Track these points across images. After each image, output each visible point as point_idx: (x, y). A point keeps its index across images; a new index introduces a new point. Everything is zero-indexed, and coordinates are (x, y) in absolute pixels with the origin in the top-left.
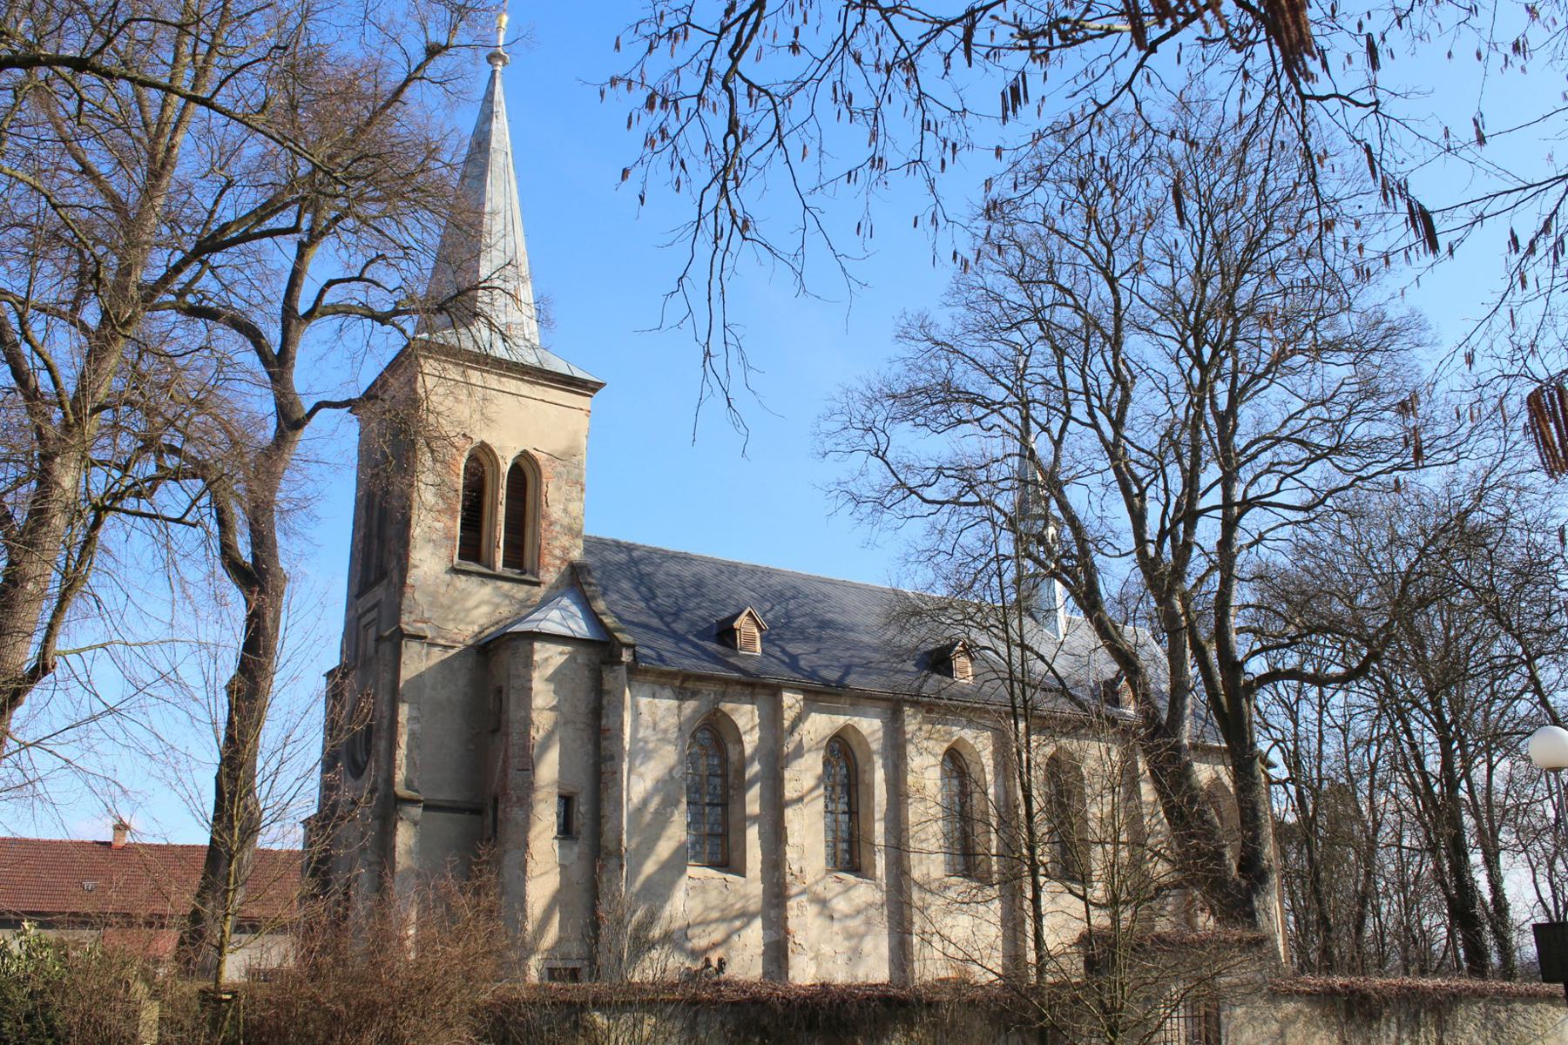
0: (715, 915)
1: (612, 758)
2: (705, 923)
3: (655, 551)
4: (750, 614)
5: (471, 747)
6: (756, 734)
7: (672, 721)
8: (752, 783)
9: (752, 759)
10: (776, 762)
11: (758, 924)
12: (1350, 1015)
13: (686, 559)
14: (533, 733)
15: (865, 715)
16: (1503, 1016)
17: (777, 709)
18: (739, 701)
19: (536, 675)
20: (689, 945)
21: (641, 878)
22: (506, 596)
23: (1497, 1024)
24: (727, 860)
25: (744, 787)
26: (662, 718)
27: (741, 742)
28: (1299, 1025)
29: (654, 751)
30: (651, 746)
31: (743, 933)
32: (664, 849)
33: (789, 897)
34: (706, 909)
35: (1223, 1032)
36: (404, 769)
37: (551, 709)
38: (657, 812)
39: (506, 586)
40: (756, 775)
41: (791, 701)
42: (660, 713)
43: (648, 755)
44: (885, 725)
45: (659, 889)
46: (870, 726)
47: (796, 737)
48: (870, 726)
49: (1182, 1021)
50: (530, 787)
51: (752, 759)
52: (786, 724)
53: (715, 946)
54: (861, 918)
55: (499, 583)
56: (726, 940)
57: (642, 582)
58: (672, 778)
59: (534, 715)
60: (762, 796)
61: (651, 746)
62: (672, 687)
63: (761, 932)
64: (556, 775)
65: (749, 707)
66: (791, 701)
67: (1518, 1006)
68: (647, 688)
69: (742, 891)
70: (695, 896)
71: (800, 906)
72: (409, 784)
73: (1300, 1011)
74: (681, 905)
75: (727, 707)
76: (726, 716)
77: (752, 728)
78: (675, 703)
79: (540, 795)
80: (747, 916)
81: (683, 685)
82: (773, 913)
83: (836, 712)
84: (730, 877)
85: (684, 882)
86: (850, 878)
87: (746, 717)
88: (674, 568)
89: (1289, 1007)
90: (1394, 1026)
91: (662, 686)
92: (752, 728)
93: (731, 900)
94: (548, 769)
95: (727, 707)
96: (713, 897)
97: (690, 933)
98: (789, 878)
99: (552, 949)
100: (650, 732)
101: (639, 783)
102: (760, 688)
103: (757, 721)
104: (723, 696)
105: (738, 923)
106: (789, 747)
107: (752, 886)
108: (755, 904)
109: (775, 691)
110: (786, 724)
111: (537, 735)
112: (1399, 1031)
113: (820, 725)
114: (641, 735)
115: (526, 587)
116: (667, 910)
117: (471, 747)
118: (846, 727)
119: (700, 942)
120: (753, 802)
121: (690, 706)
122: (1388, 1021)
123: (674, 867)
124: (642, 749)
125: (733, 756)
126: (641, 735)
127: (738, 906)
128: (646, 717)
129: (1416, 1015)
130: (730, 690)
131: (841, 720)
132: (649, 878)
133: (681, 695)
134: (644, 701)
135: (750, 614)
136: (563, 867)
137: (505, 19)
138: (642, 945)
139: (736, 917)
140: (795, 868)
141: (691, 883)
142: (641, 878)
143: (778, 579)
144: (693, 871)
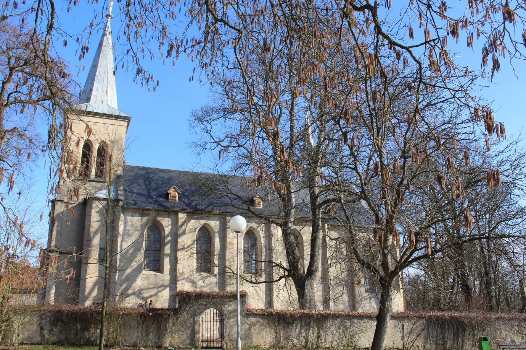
0: (152, 286)
1: (115, 236)
2: (149, 289)
3: (157, 169)
4: (174, 188)
5: (79, 234)
6: (170, 227)
7: (139, 224)
8: (167, 243)
9: (168, 236)
10: (175, 236)
11: (168, 289)
12: (279, 323)
13: (168, 171)
14: (91, 229)
15: (212, 220)
16: (348, 324)
17: (177, 219)
18: (164, 217)
19: (93, 211)
20: (142, 296)
21: (125, 275)
22: (93, 187)
23: (345, 327)
24: (159, 269)
25: (165, 245)
26: (135, 223)
27: (164, 230)
28: (258, 326)
29: (132, 233)
30: (131, 232)
31: (162, 292)
32: (134, 265)
33: (178, 281)
34: (149, 284)
35: (225, 327)
36: (54, 241)
37: (98, 221)
38: (132, 253)
39: (94, 183)
40: (169, 241)
41: (182, 216)
42: (134, 221)
43: (129, 235)
44: (220, 222)
45: (131, 278)
46: (214, 224)
47: (183, 228)
48: (214, 224)
49: (218, 323)
50: (90, 246)
51: (168, 236)
52: (180, 224)
53: (151, 296)
54: (209, 287)
55: (91, 183)
56: (156, 294)
57: (147, 179)
58: (138, 242)
59: (92, 224)
60: (171, 247)
61: (131, 232)
62: (139, 213)
63: (169, 292)
64: (99, 242)
65: (167, 218)
66: (182, 216)
67: (356, 321)
68: (130, 213)
69: (162, 279)
70: (145, 279)
71: (182, 284)
72: (56, 247)
73: (258, 321)
74: (139, 283)
75: (159, 219)
76: (159, 222)
77: (168, 226)
78: (140, 218)
79: (94, 248)
80: (164, 287)
81: (143, 212)
82: (173, 286)
83: (202, 219)
84: (158, 274)
85: (141, 276)
86: (205, 274)
87: (166, 222)
88: (162, 174)
89: (253, 320)
90: (299, 327)
91: (135, 213)
92: (168, 226)
93: (158, 281)
94: (96, 241)
95: (159, 219)
96: (152, 280)
97: (142, 292)
98: (178, 274)
99: (95, 297)
100: (130, 228)
101: (124, 244)
102: (172, 212)
103: (170, 223)
104: (158, 215)
105: (160, 289)
106: (180, 231)
107: (166, 276)
108: (167, 283)
109: (176, 213)
110: (180, 224)
111: (92, 230)
112: (301, 328)
113: (195, 224)
114: (127, 228)
115: (101, 184)
116: (134, 285)
117: (79, 234)
118: (205, 224)
119: (145, 295)
120: (167, 249)
121: (145, 219)
122: (296, 325)
123: (138, 271)
124: (127, 233)
125: (163, 235)
126: (127, 228)
127: (160, 283)
128: (129, 223)
129: (310, 323)
130: (160, 213)
131: (203, 222)
132: (129, 275)
133: (142, 215)
134: (129, 218)
135: (174, 188)
136: (100, 271)
137: (112, 3)
138: (125, 295)
139: (160, 287)
140: (181, 271)
141: (143, 276)
142: (125, 275)
143: (203, 176)
144: (145, 272)
